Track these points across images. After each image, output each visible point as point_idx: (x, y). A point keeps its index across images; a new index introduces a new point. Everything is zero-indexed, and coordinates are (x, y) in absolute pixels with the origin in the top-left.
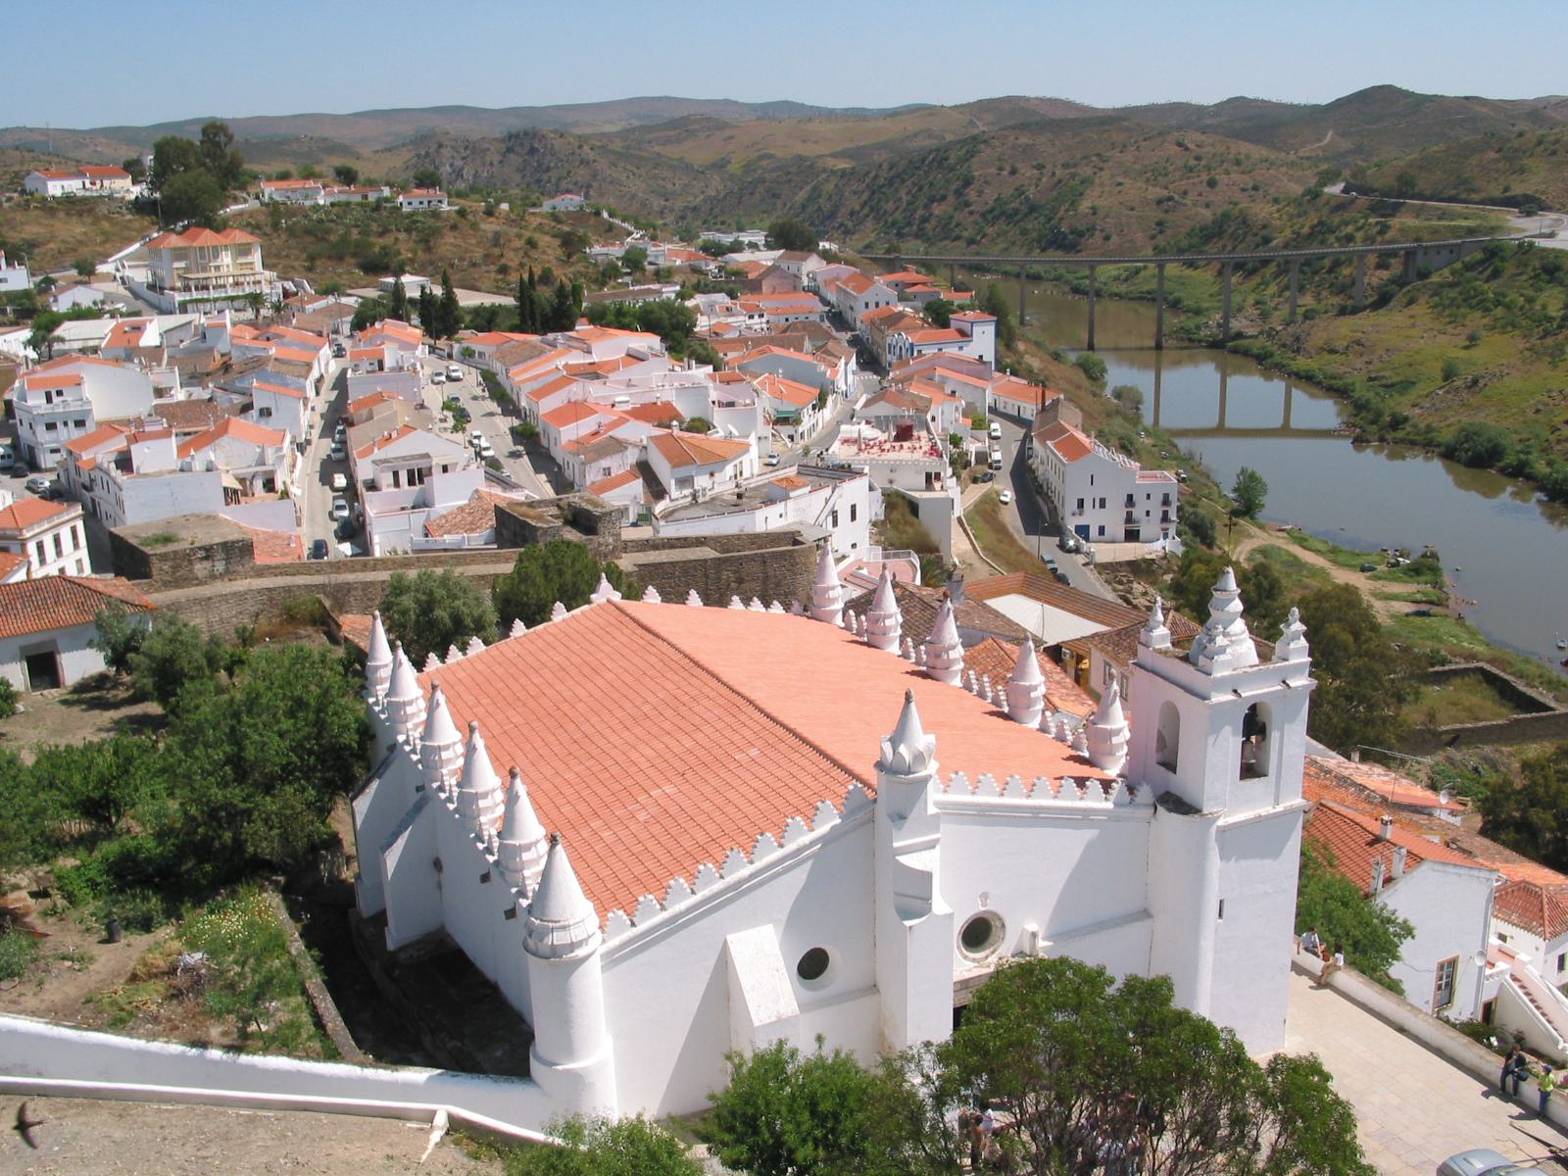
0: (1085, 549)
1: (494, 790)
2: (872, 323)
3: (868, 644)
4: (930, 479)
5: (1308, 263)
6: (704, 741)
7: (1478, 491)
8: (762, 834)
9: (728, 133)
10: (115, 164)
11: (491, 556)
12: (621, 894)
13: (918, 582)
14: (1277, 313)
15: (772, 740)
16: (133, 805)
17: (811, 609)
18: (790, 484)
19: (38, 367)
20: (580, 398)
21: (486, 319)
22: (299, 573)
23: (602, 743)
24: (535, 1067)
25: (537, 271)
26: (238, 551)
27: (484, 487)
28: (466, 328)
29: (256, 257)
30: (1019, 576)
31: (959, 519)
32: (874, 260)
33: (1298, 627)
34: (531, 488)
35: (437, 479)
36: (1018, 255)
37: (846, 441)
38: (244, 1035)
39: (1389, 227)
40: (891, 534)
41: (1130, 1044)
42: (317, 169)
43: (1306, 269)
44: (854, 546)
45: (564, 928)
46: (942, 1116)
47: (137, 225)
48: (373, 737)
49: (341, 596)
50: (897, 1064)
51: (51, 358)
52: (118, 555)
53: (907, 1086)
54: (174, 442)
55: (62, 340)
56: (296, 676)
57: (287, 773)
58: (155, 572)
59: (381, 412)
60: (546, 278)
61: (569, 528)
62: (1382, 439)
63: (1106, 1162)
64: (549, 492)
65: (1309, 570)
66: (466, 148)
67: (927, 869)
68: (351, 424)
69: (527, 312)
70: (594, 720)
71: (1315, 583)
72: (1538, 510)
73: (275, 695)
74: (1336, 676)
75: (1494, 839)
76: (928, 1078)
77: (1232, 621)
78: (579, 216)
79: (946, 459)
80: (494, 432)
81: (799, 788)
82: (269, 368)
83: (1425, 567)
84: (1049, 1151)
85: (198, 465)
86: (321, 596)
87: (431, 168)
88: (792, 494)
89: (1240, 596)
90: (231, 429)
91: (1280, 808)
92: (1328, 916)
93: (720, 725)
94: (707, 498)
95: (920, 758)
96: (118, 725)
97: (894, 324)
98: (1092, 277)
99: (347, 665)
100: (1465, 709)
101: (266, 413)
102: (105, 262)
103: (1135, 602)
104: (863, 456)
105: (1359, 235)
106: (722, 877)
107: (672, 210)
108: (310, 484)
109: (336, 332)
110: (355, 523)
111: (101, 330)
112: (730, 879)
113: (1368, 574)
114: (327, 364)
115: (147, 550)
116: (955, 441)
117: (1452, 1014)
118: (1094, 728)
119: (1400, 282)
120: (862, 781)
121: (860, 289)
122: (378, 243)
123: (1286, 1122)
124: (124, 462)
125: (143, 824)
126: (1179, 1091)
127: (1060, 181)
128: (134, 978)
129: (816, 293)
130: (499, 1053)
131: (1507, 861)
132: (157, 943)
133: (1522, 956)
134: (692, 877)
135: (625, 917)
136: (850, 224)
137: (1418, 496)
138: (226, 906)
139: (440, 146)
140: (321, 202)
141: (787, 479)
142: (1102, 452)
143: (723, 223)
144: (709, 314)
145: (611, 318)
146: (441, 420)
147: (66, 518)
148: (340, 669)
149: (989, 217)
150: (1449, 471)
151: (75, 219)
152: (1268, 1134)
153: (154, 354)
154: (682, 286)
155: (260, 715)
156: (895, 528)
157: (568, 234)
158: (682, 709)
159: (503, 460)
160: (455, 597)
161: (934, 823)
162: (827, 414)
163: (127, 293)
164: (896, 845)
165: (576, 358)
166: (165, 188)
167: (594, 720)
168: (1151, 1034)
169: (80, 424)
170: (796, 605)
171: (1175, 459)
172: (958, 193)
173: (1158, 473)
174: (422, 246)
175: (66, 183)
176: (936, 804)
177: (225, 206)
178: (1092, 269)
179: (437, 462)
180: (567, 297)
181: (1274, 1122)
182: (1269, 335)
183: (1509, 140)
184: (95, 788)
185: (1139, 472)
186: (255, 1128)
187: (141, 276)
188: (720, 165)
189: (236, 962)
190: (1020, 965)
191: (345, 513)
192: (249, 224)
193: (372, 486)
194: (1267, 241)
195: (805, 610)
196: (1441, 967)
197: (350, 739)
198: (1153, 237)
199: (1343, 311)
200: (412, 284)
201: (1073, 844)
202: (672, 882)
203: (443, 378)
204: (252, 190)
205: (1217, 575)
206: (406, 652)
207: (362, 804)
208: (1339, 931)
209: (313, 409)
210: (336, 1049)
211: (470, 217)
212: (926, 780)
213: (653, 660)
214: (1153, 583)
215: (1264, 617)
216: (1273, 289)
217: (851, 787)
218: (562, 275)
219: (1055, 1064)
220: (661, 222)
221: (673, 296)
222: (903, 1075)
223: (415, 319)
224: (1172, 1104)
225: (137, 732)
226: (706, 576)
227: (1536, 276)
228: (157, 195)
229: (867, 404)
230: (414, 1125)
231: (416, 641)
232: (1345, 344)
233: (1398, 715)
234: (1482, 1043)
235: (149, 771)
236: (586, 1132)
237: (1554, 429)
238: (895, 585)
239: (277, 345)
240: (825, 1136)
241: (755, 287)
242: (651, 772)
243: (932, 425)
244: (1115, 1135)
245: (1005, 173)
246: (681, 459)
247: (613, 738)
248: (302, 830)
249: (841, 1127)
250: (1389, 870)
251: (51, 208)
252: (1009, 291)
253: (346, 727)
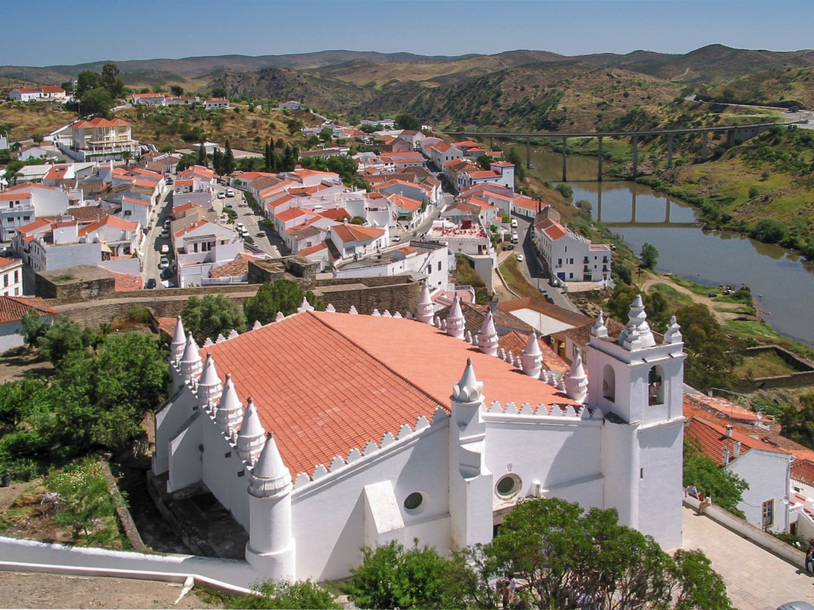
0: (563, 285)
1: (238, 409)
2: (450, 168)
3: (447, 334)
4: (481, 249)
5: (677, 137)
6: (356, 384)
7: (769, 255)
8: (386, 433)
9: (374, 69)
10: (57, 84)
11: (244, 288)
12: (306, 464)
13: (474, 302)
14: (662, 162)
15: (394, 384)
16: (28, 415)
17: (416, 315)
18: (406, 251)
19: (7, 189)
20: (296, 206)
21: (248, 166)
22: (139, 296)
23: (299, 385)
24: (249, 555)
25: (275, 139)
26: (106, 285)
27: (243, 252)
28: (237, 170)
29: (128, 133)
30: (528, 299)
31: (496, 269)
32: (451, 135)
33: (676, 326)
34: (269, 252)
35: (218, 248)
36: (525, 132)
37: (436, 229)
38: (76, 536)
39: (720, 118)
40: (460, 277)
41: (593, 544)
42: (162, 88)
43: (676, 139)
44: (440, 283)
45: (271, 481)
46: (487, 582)
47: (67, 116)
48: (171, 381)
49: (161, 308)
50: (461, 555)
51: (15, 184)
52: (39, 286)
53: (467, 567)
54: (77, 228)
55: (22, 175)
56: (132, 350)
57: (120, 400)
58: (58, 295)
59: (190, 213)
61: (288, 274)
62: (718, 228)
63: (582, 605)
64: (278, 255)
65: (681, 296)
66: (239, 77)
67: (478, 451)
68: (173, 219)
69: (269, 162)
70: (296, 373)
71: (684, 303)
72: (802, 265)
73: (119, 359)
74: (697, 352)
75: (789, 438)
76: (479, 563)
77: (641, 323)
78: (298, 113)
79: (489, 238)
80: (250, 223)
81: (408, 409)
82: (132, 190)
83: (742, 295)
84: (548, 600)
85: (89, 240)
86: (150, 308)
87: (222, 87)
88: (407, 256)
89: (645, 310)
90: (108, 221)
91: (671, 421)
92: (701, 477)
93: (365, 376)
94: (362, 258)
95: (474, 394)
96: (26, 374)
97: (462, 168)
98: (564, 144)
99: (161, 344)
100: (767, 369)
101: (128, 213)
102: (49, 135)
103: (589, 313)
104: (445, 236)
105: (704, 122)
106: (363, 455)
107: (346, 109)
108: (149, 249)
109: (169, 171)
110: (172, 271)
111: (44, 170)
112: (367, 457)
113: (713, 298)
114: (163, 188)
115: (56, 283)
116: (494, 229)
117: (773, 529)
118: (568, 377)
119: (726, 146)
120: (443, 406)
121: (444, 150)
122: (192, 126)
123: (687, 586)
124: (49, 238)
125: (33, 425)
126: (623, 568)
127: (547, 94)
128: (15, 506)
129: (421, 152)
130: (227, 547)
131: (796, 449)
132: (31, 488)
133: (810, 500)
134: (346, 455)
135: (307, 476)
136: (438, 116)
137: (738, 257)
138: (75, 468)
139: (226, 76)
140: (164, 105)
141: (404, 248)
142: (571, 235)
143: (372, 116)
144: (364, 163)
145: (313, 165)
146: (222, 218)
147: (13, 266)
148: (157, 346)
149: (510, 113)
150: (754, 245)
151: (34, 114)
152: (676, 591)
153: (71, 183)
154: (351, 148)
155: (108, 369)
156: (462, 274)
157: (293, 121)
158: (345, 368)
159: (254, 238)
160: (224, 309)
161: (482, 428)
162: (426, 215)
163: (59, 151)
164: (461, 439)
165: (295, 186)
166: (83, 97)
167: (296, 373)
168: (606, 539)
169: (27, 218)
170: (408, 314)
171: (609, 238)
172: (494, 100)
173: (600, 245)
174: (215, 127)
175: (31, 95)
176: (484, 418)
177: (113, 107)
178: (565, 140)
179: (219, 239)
180: (290, 154)
181: (680, 585)
182: (658, 174)
183: (783, 73)
184: (8, 406)
185: (590, 245)
186: (77, 585)
187: (67, 142)
188: (371, 86)
189: (77, 498)
190: (530, 502)
191: (167, 265)
192: (125, 116)
193: (183, 251)
194: (656, 125)
195: (413, 316)
196: (765, 504)
197: (158, 382)
198: (596, 123)
199: (696, 162)
200: (209, 147)
201: (560, 439)
202: (334, 458)
203: (224, 196)
204: (128, 99)
205: (633, 298)
206: (194, 337)
207: (161, 417)
208: (707, 485)
209: (154, 211)
210: (131, 544)
211: (241, 113)
212: (478, 405)
213: (330, 342)
214: (598, 303)
215: (658, 321)
216: (659, 150)
217: (437, 409)
218: (288, 142)
219: (551, 554)
220: (340, 115)
221: (346, 153)
222: (465, 561)
224: (620, 575)
225: (38, 377)
226: (361, 299)
227: (798, 144)
228: (79, 101)
229: (447, 210)
230: (173, 585)
231: (200, 332)
232: (698, 178)
233: (732, 372)
234: (792, 545)
235: (41, 397)
236: (275, 589)
237: (809, 223)
238: (462, 304)
239: (136, 178)
240: (417, 592)
241: (389, 149)
242: (327, 401)
243: (481, 221)
244: (587, 591)
245: (518, 90)
246: (348, 237)
248: (125, 429)
249: (427, 587)
250: (731, 453)
251: (22, 107)
252: (521, 151)
253: (157, 376)
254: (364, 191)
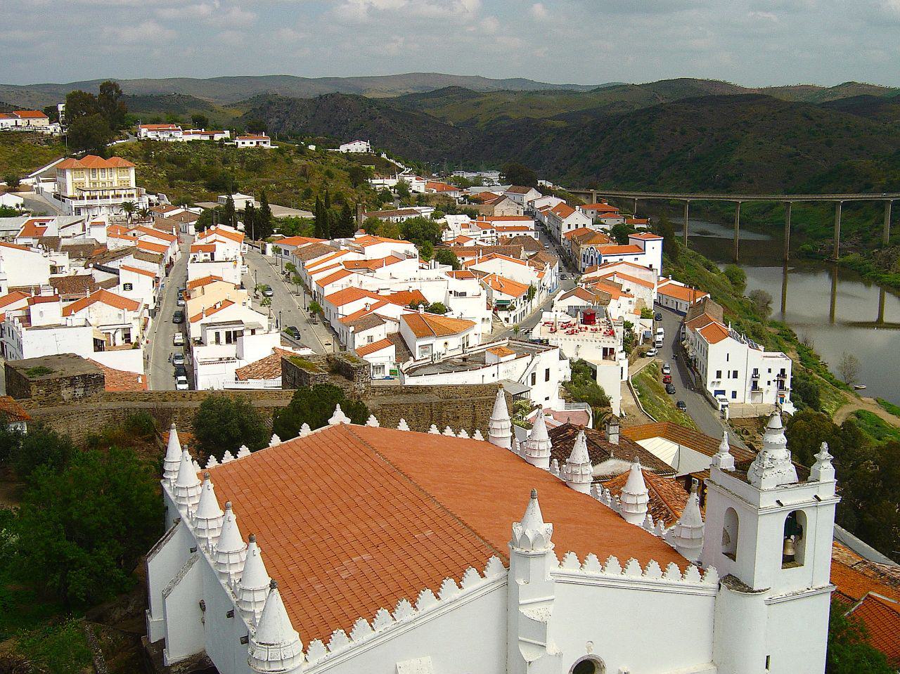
12: (322, 629)
21: (292, 229)
58: (33, 393)
60: (339, 199)
93: (407, 513)
124: (26, 320)
158: (383, 502)
223: (241, 226)
242: (355, 544)
247: (333, 520)
254: (450, 268)
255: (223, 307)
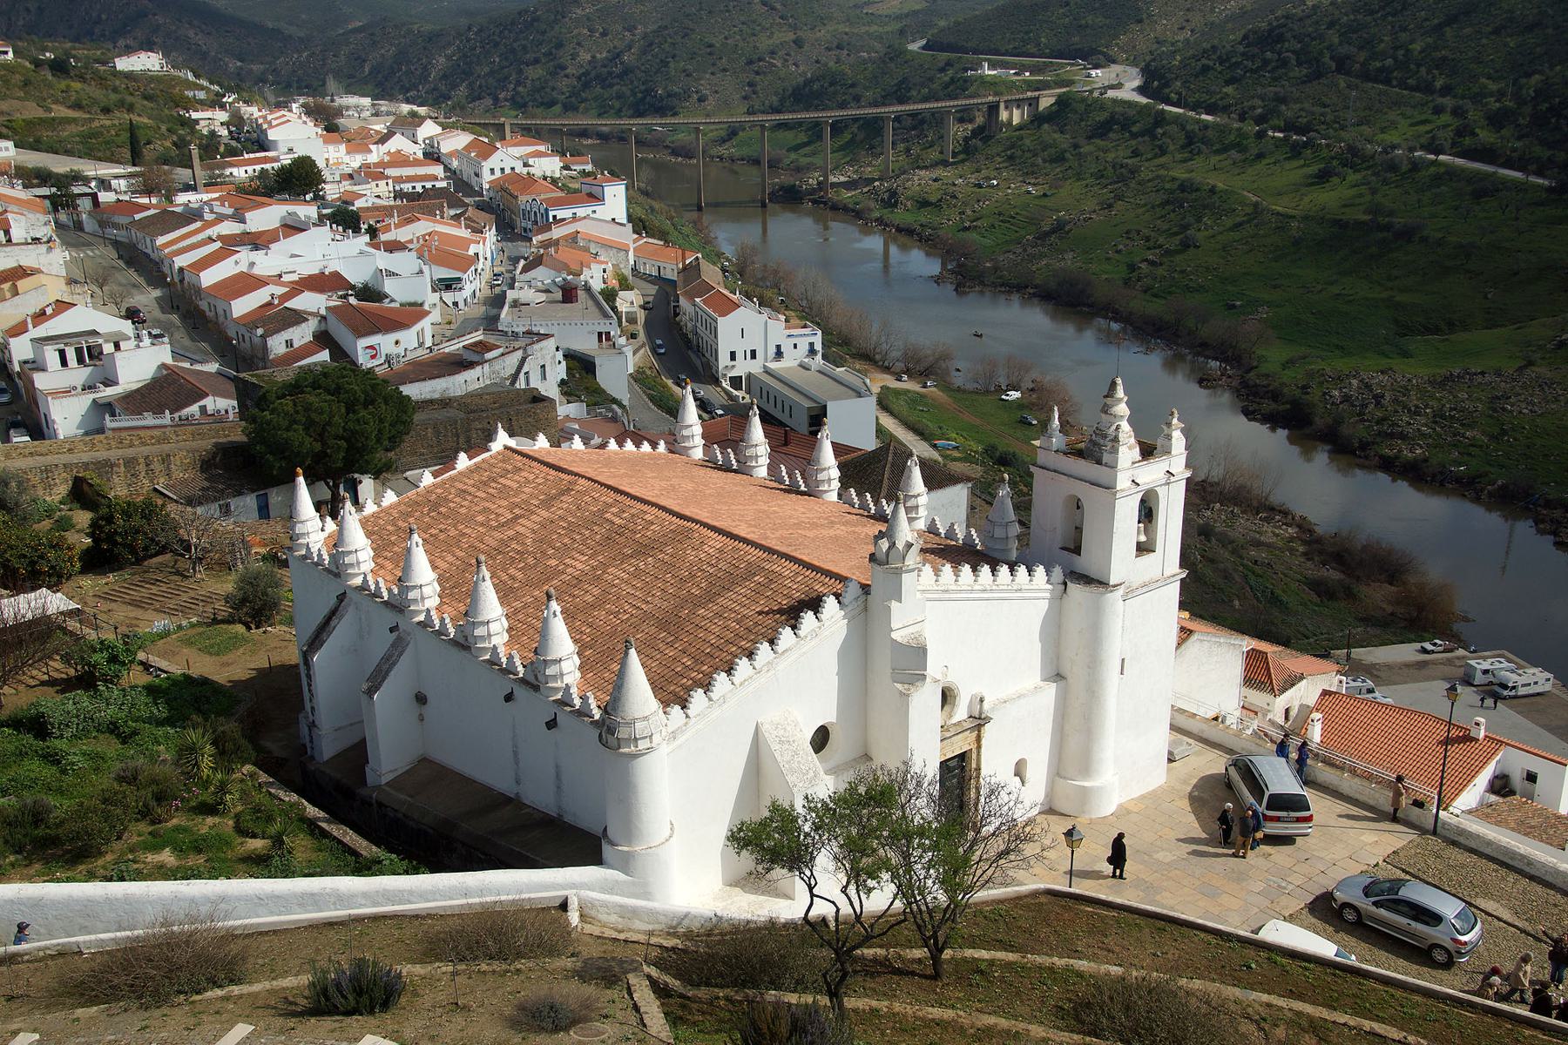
255: (56, 313)
